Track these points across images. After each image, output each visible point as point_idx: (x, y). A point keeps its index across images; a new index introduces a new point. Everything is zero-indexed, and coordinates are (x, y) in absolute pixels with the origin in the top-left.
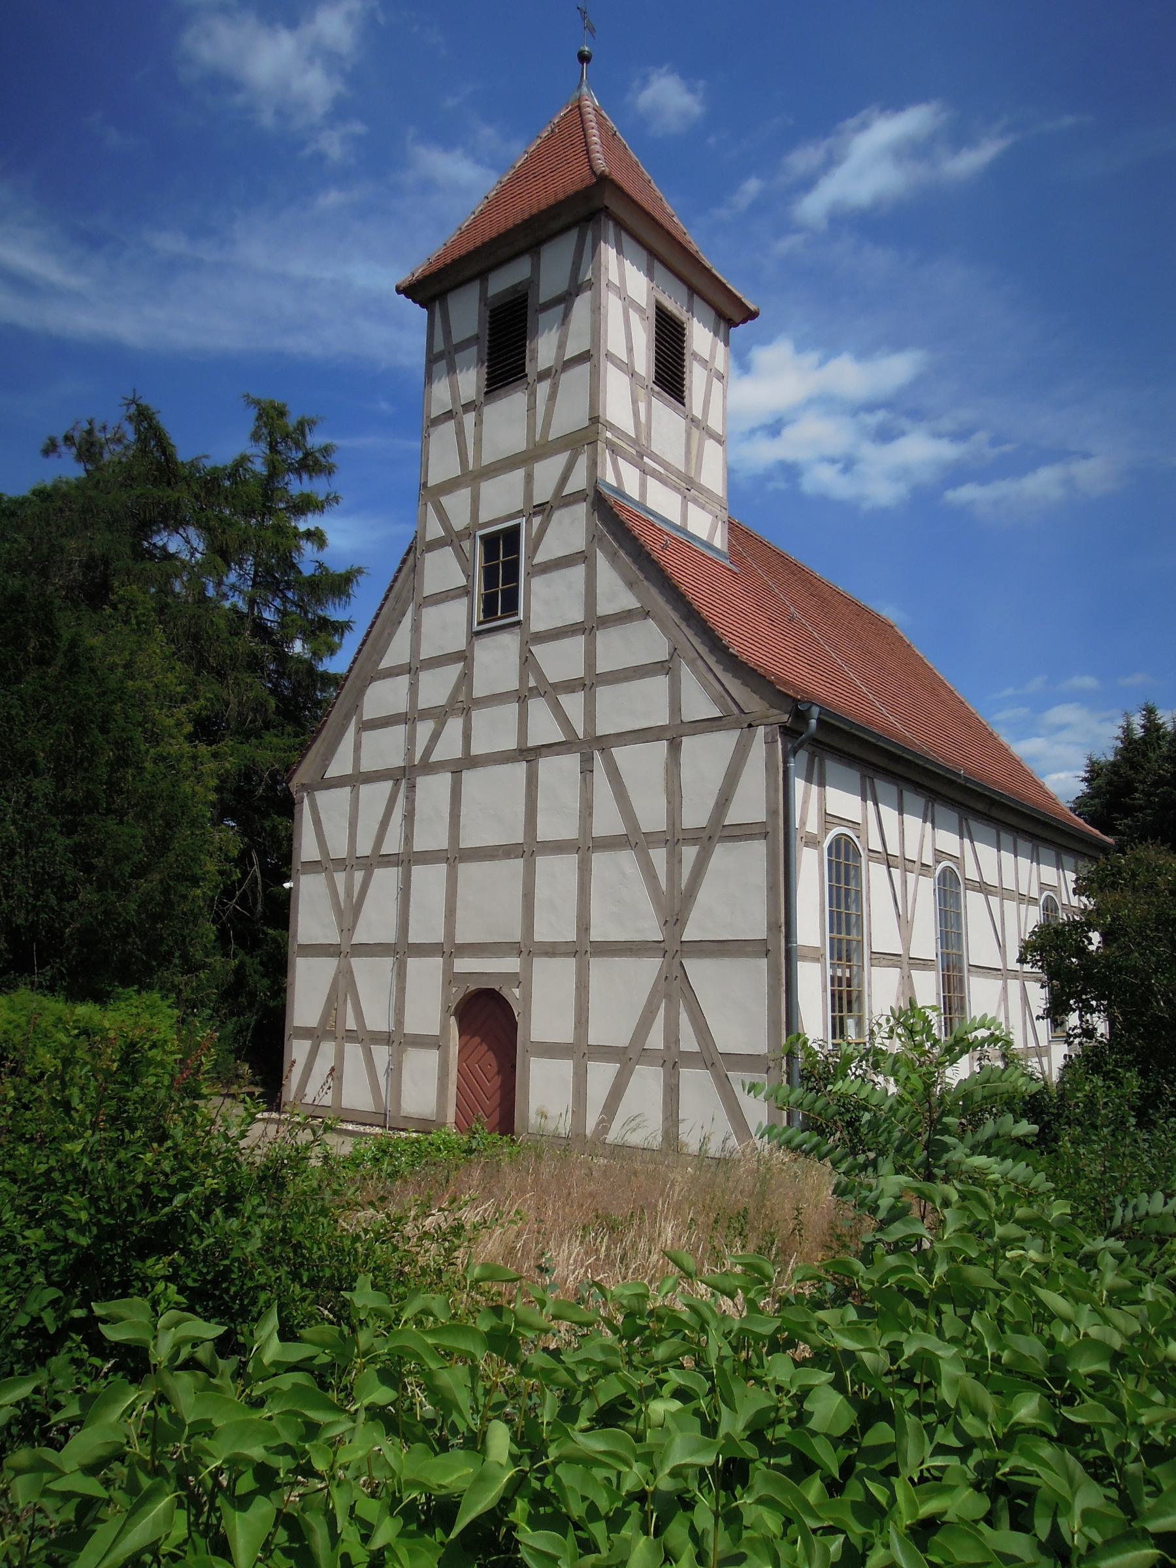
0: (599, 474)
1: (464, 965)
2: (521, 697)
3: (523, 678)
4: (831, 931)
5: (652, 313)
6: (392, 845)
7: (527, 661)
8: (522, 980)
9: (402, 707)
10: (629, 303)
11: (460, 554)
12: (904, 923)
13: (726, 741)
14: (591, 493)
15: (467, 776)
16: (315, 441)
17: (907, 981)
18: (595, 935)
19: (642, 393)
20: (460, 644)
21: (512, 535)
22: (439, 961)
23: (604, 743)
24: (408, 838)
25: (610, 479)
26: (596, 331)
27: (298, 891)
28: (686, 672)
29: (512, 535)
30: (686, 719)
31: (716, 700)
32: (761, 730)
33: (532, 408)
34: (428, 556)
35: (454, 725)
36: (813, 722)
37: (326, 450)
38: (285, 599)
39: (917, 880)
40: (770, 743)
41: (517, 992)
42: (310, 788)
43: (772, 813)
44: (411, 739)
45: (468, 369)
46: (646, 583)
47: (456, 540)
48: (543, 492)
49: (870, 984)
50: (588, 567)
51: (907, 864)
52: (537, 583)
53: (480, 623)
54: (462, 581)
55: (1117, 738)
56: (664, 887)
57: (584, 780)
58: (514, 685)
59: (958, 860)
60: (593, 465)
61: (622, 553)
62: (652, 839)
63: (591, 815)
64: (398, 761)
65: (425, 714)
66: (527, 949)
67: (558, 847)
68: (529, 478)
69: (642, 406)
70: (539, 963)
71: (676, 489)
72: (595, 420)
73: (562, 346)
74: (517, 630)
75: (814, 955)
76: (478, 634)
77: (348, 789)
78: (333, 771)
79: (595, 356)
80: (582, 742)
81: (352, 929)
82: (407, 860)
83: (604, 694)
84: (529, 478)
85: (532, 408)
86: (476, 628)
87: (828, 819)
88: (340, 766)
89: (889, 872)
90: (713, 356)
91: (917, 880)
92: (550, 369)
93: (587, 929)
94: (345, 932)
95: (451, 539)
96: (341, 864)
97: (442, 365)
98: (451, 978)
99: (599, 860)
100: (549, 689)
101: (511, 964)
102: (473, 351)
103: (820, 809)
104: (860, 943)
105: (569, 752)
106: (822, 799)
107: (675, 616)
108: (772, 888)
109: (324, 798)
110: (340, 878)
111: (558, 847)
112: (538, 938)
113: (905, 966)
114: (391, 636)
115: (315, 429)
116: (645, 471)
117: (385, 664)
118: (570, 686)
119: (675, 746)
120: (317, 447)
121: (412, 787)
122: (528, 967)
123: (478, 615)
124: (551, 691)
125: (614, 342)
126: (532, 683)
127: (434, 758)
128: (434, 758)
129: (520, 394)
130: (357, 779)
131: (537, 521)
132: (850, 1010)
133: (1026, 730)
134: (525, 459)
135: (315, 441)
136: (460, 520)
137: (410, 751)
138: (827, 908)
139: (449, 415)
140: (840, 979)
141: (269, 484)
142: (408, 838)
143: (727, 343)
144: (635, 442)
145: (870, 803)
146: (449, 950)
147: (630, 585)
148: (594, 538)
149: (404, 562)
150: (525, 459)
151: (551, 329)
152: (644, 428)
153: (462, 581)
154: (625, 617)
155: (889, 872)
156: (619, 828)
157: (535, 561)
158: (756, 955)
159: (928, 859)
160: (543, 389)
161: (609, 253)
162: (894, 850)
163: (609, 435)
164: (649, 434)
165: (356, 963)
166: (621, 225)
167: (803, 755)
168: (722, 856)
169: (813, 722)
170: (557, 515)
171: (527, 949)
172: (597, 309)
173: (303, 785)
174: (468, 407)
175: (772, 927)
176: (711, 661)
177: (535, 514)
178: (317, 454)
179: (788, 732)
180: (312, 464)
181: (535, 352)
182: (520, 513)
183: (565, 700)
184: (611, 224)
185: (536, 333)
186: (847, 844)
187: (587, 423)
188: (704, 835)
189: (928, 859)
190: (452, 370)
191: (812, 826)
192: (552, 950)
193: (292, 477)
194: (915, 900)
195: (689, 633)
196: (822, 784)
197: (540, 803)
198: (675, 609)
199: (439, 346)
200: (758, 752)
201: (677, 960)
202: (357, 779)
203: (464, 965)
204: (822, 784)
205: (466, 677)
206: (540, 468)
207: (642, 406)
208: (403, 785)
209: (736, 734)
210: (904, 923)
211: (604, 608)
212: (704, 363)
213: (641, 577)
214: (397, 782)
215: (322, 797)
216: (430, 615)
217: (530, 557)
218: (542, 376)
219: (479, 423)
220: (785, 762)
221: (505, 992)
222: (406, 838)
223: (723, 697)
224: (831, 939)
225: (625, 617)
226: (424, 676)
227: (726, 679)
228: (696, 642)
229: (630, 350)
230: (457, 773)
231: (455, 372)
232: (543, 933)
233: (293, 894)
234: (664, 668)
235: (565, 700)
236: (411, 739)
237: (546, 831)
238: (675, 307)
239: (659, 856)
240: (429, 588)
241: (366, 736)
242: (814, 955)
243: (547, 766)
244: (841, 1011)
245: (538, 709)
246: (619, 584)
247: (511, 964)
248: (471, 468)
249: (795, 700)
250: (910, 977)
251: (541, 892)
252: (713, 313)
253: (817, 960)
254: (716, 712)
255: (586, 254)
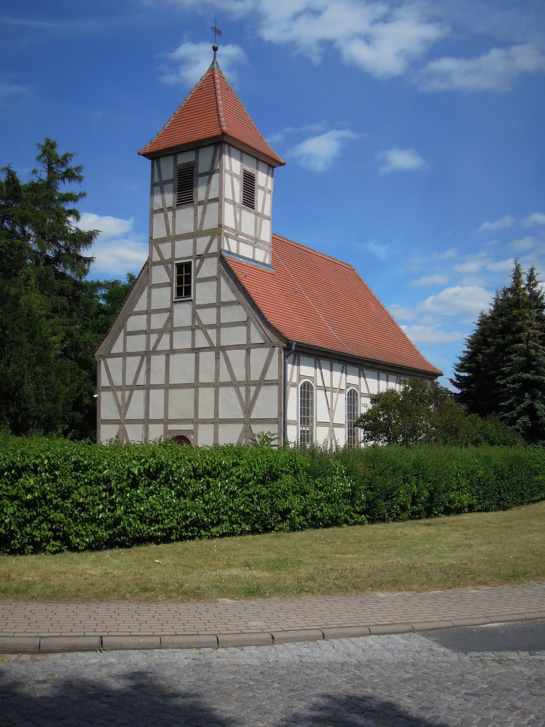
0: (222, 247)
1: (171, 427)
2: (193, 329)
3: (193, 322)
4: (301, 415)
5: (242, 176)
6: (141, 381)
7: (195, 315)
8: (194, 432)
9: (144, 327)
10: (232, 175)
11: (167, 269)
12: (331, 411)
13: (265, 351)
14: (219, 254)
15: (172, 357)
16: (72, 164)
17: (332, 432)
18: (221, 416)
19: (238, 209)
20: (168, 305)
21: (188, 266)
22: (162, 426)
23: (224, 349)
24: (148, 379)
25: (226, 248)
26: (221, 190)
27: (100, 398)
28: (252, 326)
29: (188, 266)
30: (252, 342)
31: (262, 337)
32: (277, 349)
33: (196, 215)
34: (153, 268)
35: (166, 337)
36: (294, 347)
37: (78, 169)
38: (58, 245)
39: (337, 396)
40: (280, 353)
41: (192, 436)
42: (104, 357)
43: (280, 377)
44: (148, 341)
45: (169, 193)
46: (239, 292)
47: (165, 264)
48: (201, 251)
49: (316, 433)
50: (218, 282)
51: (333, 390)
52: (198, 285)
53: (176, 298)
54: (168, 281)
55: (491, 304)
56: (244, 400)
57: (216, 361)
58: (190, 324)
59: (359, 387)
60: (220, 244)
61: (230, 279)
62: (240, 383)
63: (219, 374)
64: (143, 349)
65: (154, 331)
66: (196, 421)
67: (207, 385)
68: (195, 244)
69: (238, 215)
70: (201, 427)
71: (251, 244)
72: (220, 226)
73: (207, 193)
74: (191, 303)
75: (294, 423)
76: (175, 302)
77: (121, 358)
78: (114, 351)
79: (220, 201)
80: (215, 348)
81: (125, 414)
82: (148, 387)
83: (223, 331)
84: (195, 244)
85: (196, 215)
86: (174, 300)
87: (300, 377)
88: (117, 348)
89: (326, 393)
90: (266, 184)
91: (337, 396)
92: (203, 201)
93: (218, 414)
94: (122, 415)
95: (163, 262)
96: (119, 388)
97: (157, 189)
98: (166, 432)
99: (222, 390)
100: (203, 327)
101: (190, 427)
102: (171, 186)
103: (298, 374)
104: (312, 419)
105: (211, 351)
106: (299, 370)
107: (249, 305)
108: (279, 402)
109: (110, 361)
110: (119, 394)
111: (207, 385)
112: (200, 417)
113: (331, 426)
114: (138, 298)
115: (72, 158)
116: (238, 241)
117: (136, 309)
118: (211, 327)
119: (248, 352)
120: (73, 167)
121: (149, 360)
122: (196, 428)
123: (175, 295)
124: (204, 328)
125: (228, 194)
126: (197, 324)
127: (158, 349)
128: (158, 349)
129: (191, 208)
130: (125, 355)
131: (198, 261)
132: (308, 441)
133: (410, 324)
134: (195, 235)
135: (72, 164)
136: (167, 256)
137: (148, 345)
138: (299, 407)
139: (161, 210)
140: (304, 431)
141: (50, 184)
142: (148, 379)
143: (272, 177)
144: (235, 231)
145: (318, 369)
146: (166, 421)
147: (233, 292)
148: (219, 272)
149: (143, 268)
150: (195, 235)
151: (203, 185)
152: (238, 224)
153: (168, 281)
154: (231, 303)
155: (326, 393)
156: (229, 379)
157: (197, 277)
158: (274, 423)
159: (343, 387)
160: (200, 208)
161: (226, 158)
162: (328, 384)
163: (225, 231)
164: (240, 226)
165: (127, 426)
166: (230, 145)
167: (291, 357)
168: (264, 390)
169: (294, 347)
170: (206, 261)
171: (196, 421)
172: (221, 181)
173: (100, 355)
174: (169, 209)
175: (280, 414)
176: (261, 323)
177: (197, 258)
178: (74, 171)
179: (285, 349)
180: (70, 175)
181: (197, 193)
182: (191, 257)
183: (209, 331)
184: (227, 146)
185: (197, 185)
186: (308, 385)
187: (217, 227)
188: (258, 383)
189: (343, 387)
190: (162, 192)
191: (295, 380)
192: (205, 422)
193: (60, 182)
194: (336, 402)
195: (254, 312)
196: (299, 365)
197: (201, 368)
198: (248, 302)
199: (156, 180)
200: (276, 356)
201: (248, 425)
202: (125, 355)
203: (171, 427)
204: (299, 365)
205: (171, 319)
206: (199, 240)
207: (238, 215)
208: (145, 358)
209: (269, 349)
210: (331, 411)
211: (224, 299)
212: (263, 188)
213: (237, 289)
214: (143, 357)
215: (110, 361)
216: (155, 292)
217: (196, 275)
218: (200, 203)
219: (174, 216)
220: (285, 360)
221: (188, 437)
222: (147, 379)
223: (263, 337)
224: (301, 418)
225: (231, 303)
226: (153, 316)
227: (266, 330)
228: (256, 316)
229: (233, 194)
230: (168, 355)
231: (163, 193)
232: (201, 416)
233: (98, 399)
234: (245, 323)
235: (209, 331)
236: (148, 341)
237: (203, 379)
238: (250, 170)
239: (243, 389)
240: (155, 281)
241: (129, 338)
242: (294, 423)
243: (203, 355)
244: (304, 441)
245: (199, 334)
246: (229, 291)
247: (190, 427)
248: (171, 235)
249: (288, 339)
250: (333, 430)
251: (201, 401)
252: (267, 166)
253: (295, 425)
254: (262, 341)
255: (216, 159)
